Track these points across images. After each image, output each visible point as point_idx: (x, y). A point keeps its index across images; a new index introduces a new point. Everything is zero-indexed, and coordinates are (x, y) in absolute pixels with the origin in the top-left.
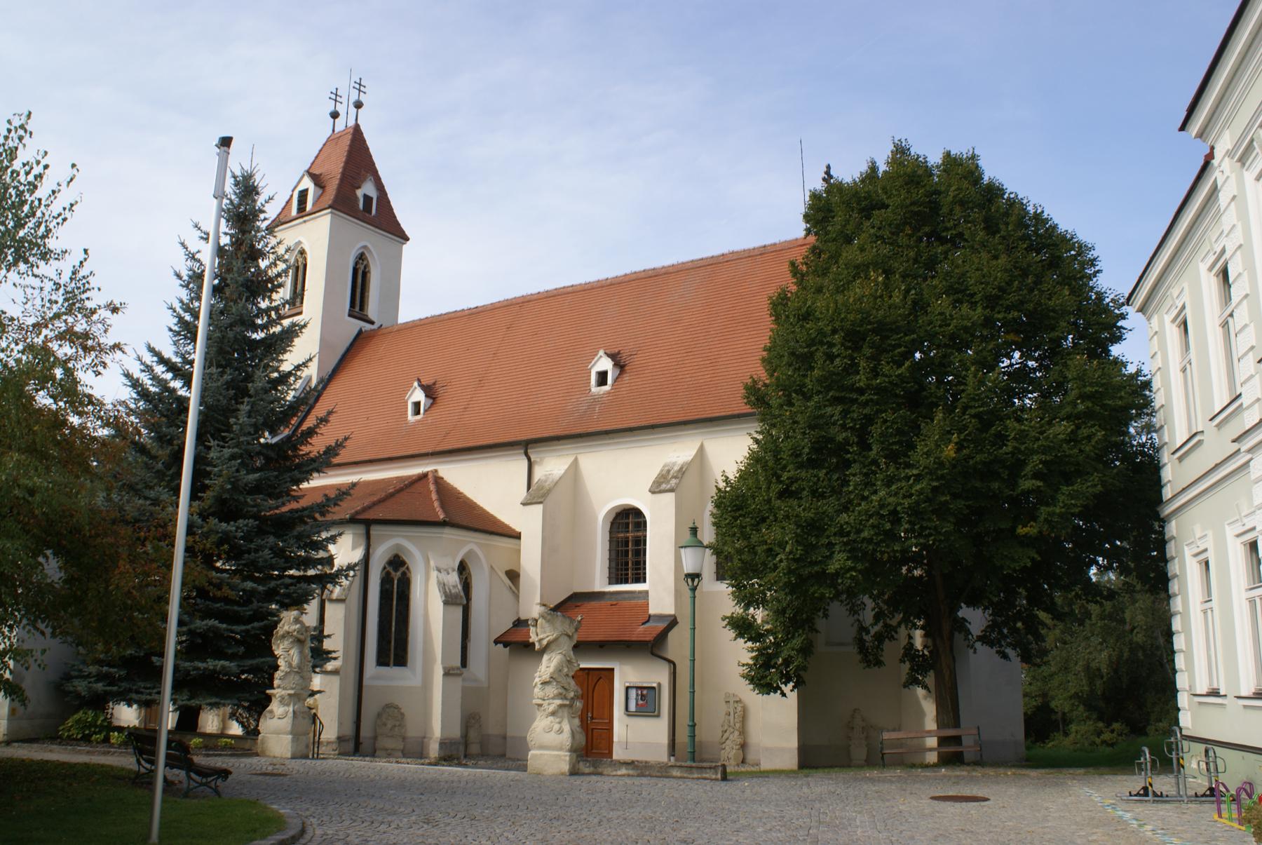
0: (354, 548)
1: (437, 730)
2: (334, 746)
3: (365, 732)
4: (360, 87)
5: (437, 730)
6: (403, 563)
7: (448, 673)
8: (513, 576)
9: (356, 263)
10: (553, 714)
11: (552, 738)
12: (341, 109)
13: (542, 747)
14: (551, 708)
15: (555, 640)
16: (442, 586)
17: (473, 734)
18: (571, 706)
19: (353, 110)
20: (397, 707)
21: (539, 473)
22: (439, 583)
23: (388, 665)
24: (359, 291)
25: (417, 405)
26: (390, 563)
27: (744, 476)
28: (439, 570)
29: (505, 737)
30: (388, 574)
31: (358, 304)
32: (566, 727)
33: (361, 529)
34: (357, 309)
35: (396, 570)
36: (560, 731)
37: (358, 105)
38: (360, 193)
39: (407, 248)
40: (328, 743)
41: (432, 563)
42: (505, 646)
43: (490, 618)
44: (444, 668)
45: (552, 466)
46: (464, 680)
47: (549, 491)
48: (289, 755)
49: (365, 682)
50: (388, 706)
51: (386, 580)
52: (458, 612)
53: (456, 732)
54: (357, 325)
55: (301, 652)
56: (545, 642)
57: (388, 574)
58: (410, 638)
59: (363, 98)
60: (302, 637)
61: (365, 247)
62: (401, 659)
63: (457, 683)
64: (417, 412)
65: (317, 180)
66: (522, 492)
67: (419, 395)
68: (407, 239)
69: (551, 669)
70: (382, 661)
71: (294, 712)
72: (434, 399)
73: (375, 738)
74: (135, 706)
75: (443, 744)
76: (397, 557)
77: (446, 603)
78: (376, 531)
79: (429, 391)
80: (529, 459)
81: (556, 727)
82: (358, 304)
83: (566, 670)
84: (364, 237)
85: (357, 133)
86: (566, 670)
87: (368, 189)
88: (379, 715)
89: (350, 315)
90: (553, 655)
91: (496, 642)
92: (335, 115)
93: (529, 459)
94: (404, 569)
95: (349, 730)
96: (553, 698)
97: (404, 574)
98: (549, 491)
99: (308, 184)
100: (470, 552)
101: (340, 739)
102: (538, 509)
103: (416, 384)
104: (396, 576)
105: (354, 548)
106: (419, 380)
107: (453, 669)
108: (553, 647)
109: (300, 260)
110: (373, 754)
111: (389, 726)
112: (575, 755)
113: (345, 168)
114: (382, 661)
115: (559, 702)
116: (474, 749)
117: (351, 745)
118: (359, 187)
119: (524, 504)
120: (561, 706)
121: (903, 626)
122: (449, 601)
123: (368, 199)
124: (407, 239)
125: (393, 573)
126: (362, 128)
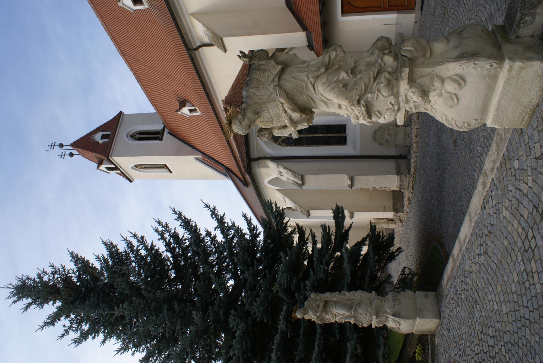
0: (267, 167)
2: (403, 177)
3: (392, 152)
4: (52, 146)
9: (136, 139)
10: (424, 93)
11: (469, 95)
12: (68, 152)
13: (484, 110)
14: (415, 98)
15: (290, 98)
18: (411, 62)
19: (64, 148)
20: (375, 132)
21: (206, 40)
23: (345, 137)
24: (149, 136)
25: (191, 111)
27: (538, 60)
31: (156, 136)
32: (454, 68)
33: (255, 164)
34: (158, 136)
36: (460, 80)
37: (61, 145)
38: (101, 142)
39: (126, 112)
45: (199, 31)
47: (214, 33)
48: (437, 321)
49: (358, 153)
50: (374, 138)
54: (166, 135)
55: (336, 304)
56: (296, 116)
58: (326, 124)
59: (57, 144)
60: (321, 305)
61: (127, 135)
64: (195, 110)
65: (100, 163)
67: (185, 110)
68: (121, 112)
69: (344, 103)
70: (342, 141)
71: (394, 315)
72: (186, 101)
73: (397, 146)
74: (374, 292)
78: (254, 154)
79: (183, 104)
80: (200, 46)
81: (450, 87)
82: (156, 136)
83: (343, 75)
84: (122, 138)
85: (75, 145)
86: (343, 75)
87: (98, 137)
88: (380, 144)
89: (162, 140)
90: (317, 98)
92: (71, 155)
93: (200, 46)
95: (391, 164)
96: (397, 95)
98: (214, 33)
99: (103, 167)
101: (398, 173)
102: (226, 40)
103: (179, 113)
105: (267, 167)
106: (177, 111)
108: (303, 99)
109: (140, 167)
110: (409, 148)
111: (388, 137)
112: (507, 48)
113: (90, 151)
114: (342, 141)
115: (404, 86)
117: (402, 162)
118: (98, 142)
119: (225, 51)
120: (412, 81)
121: (394, 251)
123: (103, 137)
124: (121, 112)
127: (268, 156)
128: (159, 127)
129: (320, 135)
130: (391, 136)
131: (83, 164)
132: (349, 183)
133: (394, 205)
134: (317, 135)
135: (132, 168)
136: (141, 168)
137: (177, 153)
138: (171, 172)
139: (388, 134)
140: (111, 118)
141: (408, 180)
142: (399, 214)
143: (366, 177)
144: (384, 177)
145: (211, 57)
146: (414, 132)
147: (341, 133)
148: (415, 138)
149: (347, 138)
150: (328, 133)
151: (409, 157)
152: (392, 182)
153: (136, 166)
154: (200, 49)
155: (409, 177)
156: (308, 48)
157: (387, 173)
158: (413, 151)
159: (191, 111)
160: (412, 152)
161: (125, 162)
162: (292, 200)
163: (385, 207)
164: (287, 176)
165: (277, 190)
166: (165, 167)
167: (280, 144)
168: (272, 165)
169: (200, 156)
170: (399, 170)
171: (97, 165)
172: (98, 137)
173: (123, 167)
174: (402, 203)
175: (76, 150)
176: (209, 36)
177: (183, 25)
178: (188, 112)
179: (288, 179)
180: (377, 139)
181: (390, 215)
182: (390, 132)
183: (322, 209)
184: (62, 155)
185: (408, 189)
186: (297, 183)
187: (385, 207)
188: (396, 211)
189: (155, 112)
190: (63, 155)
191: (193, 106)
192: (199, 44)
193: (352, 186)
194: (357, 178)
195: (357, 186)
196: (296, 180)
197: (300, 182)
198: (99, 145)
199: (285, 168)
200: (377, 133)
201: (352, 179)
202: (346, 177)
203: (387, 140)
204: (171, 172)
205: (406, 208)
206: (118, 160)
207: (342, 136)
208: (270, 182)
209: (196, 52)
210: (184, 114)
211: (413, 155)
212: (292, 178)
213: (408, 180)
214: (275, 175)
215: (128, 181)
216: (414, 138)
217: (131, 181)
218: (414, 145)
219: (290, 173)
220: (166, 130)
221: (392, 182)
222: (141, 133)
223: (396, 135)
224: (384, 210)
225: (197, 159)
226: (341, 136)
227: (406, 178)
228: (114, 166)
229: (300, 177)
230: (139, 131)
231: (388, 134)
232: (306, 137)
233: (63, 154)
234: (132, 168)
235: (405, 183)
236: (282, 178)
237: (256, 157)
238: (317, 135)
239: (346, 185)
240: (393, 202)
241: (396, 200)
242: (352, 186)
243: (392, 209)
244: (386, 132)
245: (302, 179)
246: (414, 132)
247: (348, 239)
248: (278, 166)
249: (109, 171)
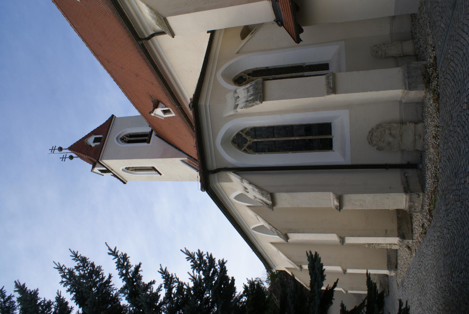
0: (230, 181)
1: (397, 93)
2: (415, 196)
3: (396, 159)
4: (53, 150)
5: (397, 93)
6: (238, 135)
7: (333, 89)
8: (246, 31)
12: (68, 155)
16: (249, 103)
17: (394, 51)
19: (63, 151)
20: (371, 133)
22: (246, 107)
23: (331, 140)
25: (165, 112)
26: (240, 147)
28: (236, 106)
29: (393, 17)
30: (249, 147)
31: (143, 138)
33: (213, 178)
34: (147, 138)
35: (246, 141)
37: (60, 149)
38: (93, 145)
39: (117, 115)
40: (411, 201)
41: (232, 113)
42: (302, 31)
43: (277, 49)
44: (328, 93)
45: (146, 16)
46: (340, 71)
49: (348, 162)
50: (370, 142)
51: (257, 149)
52: (272, 85)
53: (396, 73)
57: (249, 147)
59: (57, 148)
61: (117, 138)
62: (325, 128)
63: (343, 78)
66: (167, 37)
67: (159, 112)
68: (113, 116)
70: (327, 145)
73: (403, 151)
75: (410, 86)
76: (234, 141)
77: (263, 99)
78: (212, 164)
79: (156, 106)
80: (153, 35)
82: (143, 138)
85: (71, 148)
87: (91, 141)
88: (379, 149)
89: (149, 142)
91: (298, 40)
92: (71, 157)
93: (153, 35)
94: (244, 136)
95: (395, 177)
97: (248, 133)
99: (96, 170)
100: (224, 76)
101: (407, 190)
103: (152, 114)
104: (250, 140)
105: (230, 181)
107: (328, 84)
109: (131, 169)
110: (421, 154)
111: (391, 139)
114: (327, 145)
116: (408, 47)
117: (411, 173)
118: (91, 146)
122: (260, 95)
123: (96, 140)
124: (113, 116)
125: (248, 143)
126: (69, 146)
127: (230, 166)
128: (147, 129)
129: (297, 138)
130: (394, 137)
131: (81, 165)
132: (336, 203)
133: (399, 228)
134: (293, 138)
135: (123, 170)
136: (132, 170)
137: (164, 155)
138: (161, 174)
139: (391, 134)
140: (104, 121)
141: (422, 201)
142: (406, 241)
143: (360, 196)
144: (386, 195)
145: (165, 45)
146: (431, 131)
147: (325, 134)
148: (433, 141)
149: (333, 141)
150: (307, 135)
151: (420, 166)
152: (400, 201)
153: (126, 168)
154: (154, 38)
155: (424, 196)
156: (276, 24)
157: (390, 190)
158: (430, 159)
159: (165, 112)
160: (427, 161)
161: (117, 165)
162: (266, 221)
163: (386, 231)
164: (253, 193)
165: (248, 206)
166: (153, 169)
167: (245, 151)
168: (233, 177)
169: (185, 159)
170: (408, 186)
171: (91, 166)
172: (91, 141)
173: (114, 169)
174: (410, 226)
175: (76, 154)
176: (155, 19)
177: (128, 9)
178: (162, 114)
179: (256, 198)
180: (374, 143)
181: (395, 240)
182: (393, 132)
183: (304, 233)
184: (63, 158)
185: (421, 212)
186: (267, 204)
187: (386, 231)
188: (402, 236)
189: (140, 114)
190: (64, 158)
191: (166, 107)
192: (151, 33)
193: (340, 207)
194: (347, 198)
195: (347, 206)
196: (264, 199)
197: (270, 202)
198: (91, 149)
199: (250, 183)
200: (375, 134)
201: (340, 199)
202: (331, 196)
203: (389, 143)
204: (161, 174)
205: (416, 235)
206: (109, 163)
207: (327, 139)
208: (237, 198)
209: (149, 41)
210: (157, 115)
211: (429, 165)
212: (259, 196)
213: (422, 201)
214: (240, 191)
215: (122, 183)
216: (431, 141)
217: (125, 183)
218: (432, 150)
219: (256, 190)
220: (154, 132)
221: (400, 201)
222: (131, 136)
223: (401, 136)
224: (386, 234)
225: (183, 161)
226: (325, 139)
227: (419, 196)
228: (104, 169)
229: (269, 195)
230: (129, 134)
231: (391, 134)
232: (293, 136)
233: (64, 157)
234: (123, 170)
235: (416, 204)
236: (248, 195)
237: (215, 167)
238: (293, 138)
239: (333, 207)
240: (398, 224)
241: (403, 223)
242: (340, 207)
243: (396, 233)
244: (387, 132)
245: (272, 197)
246: (431, 131)
247: (332, 299)
248: (242, 180)
249: (102, 174)
